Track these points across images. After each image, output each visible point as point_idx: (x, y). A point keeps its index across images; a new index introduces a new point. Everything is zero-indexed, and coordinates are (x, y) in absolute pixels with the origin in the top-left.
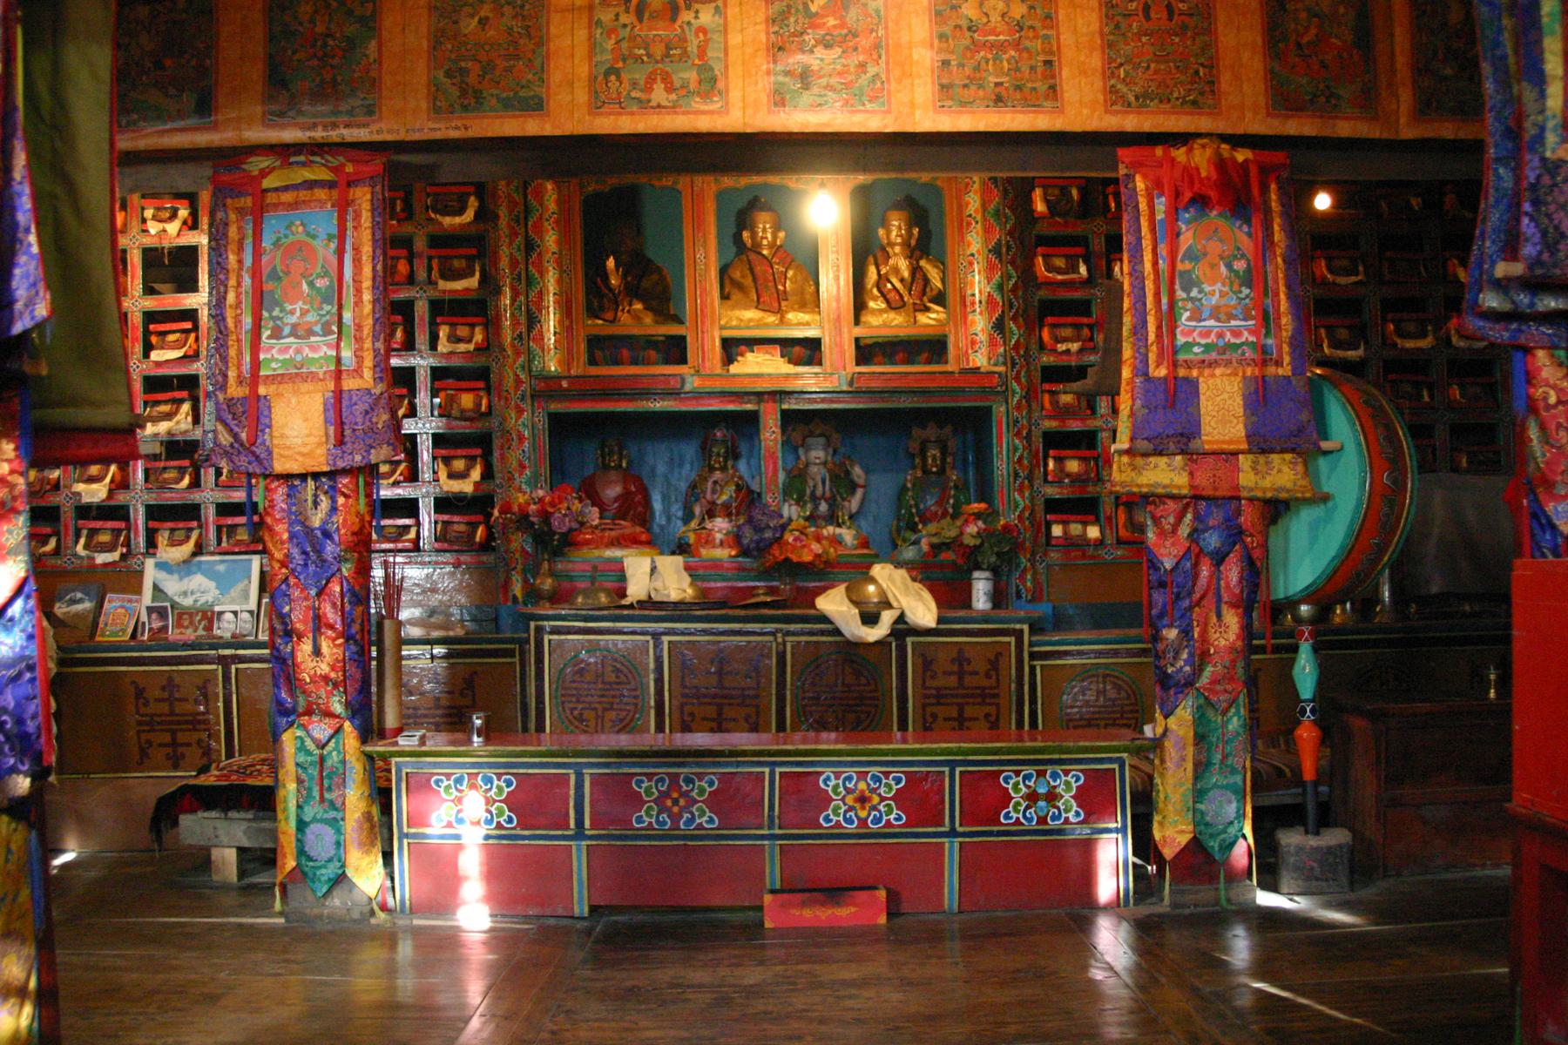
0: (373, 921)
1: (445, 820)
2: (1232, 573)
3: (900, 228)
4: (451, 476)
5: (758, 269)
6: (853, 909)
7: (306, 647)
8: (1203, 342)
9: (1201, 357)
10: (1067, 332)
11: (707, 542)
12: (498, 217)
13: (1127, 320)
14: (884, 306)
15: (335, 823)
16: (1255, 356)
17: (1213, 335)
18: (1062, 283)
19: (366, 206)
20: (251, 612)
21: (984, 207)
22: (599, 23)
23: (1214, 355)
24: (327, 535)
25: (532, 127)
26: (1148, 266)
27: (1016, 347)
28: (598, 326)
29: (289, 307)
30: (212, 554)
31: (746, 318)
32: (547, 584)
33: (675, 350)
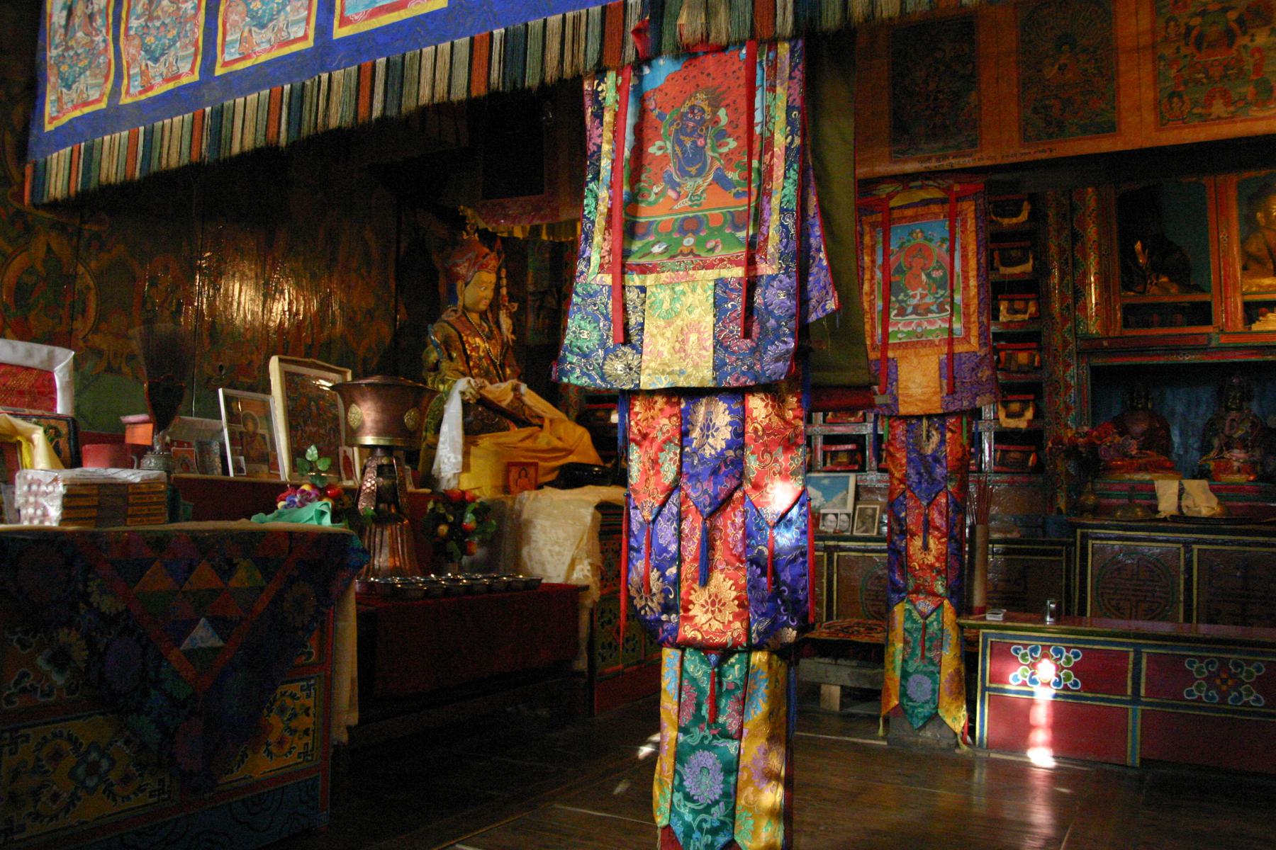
0: (957, 751)
1: (1021, 679)
4: (1009, 416)
7: (918, 542)
12: (1047, 215)
15: (932, 675)
20: (848, 515)
22: (1161, 57)
24: (936, 460)
25: (1106, 145)
29: (911, 293)
30: (819, 471)
32: (1091, 500)
33: (1202, 314)
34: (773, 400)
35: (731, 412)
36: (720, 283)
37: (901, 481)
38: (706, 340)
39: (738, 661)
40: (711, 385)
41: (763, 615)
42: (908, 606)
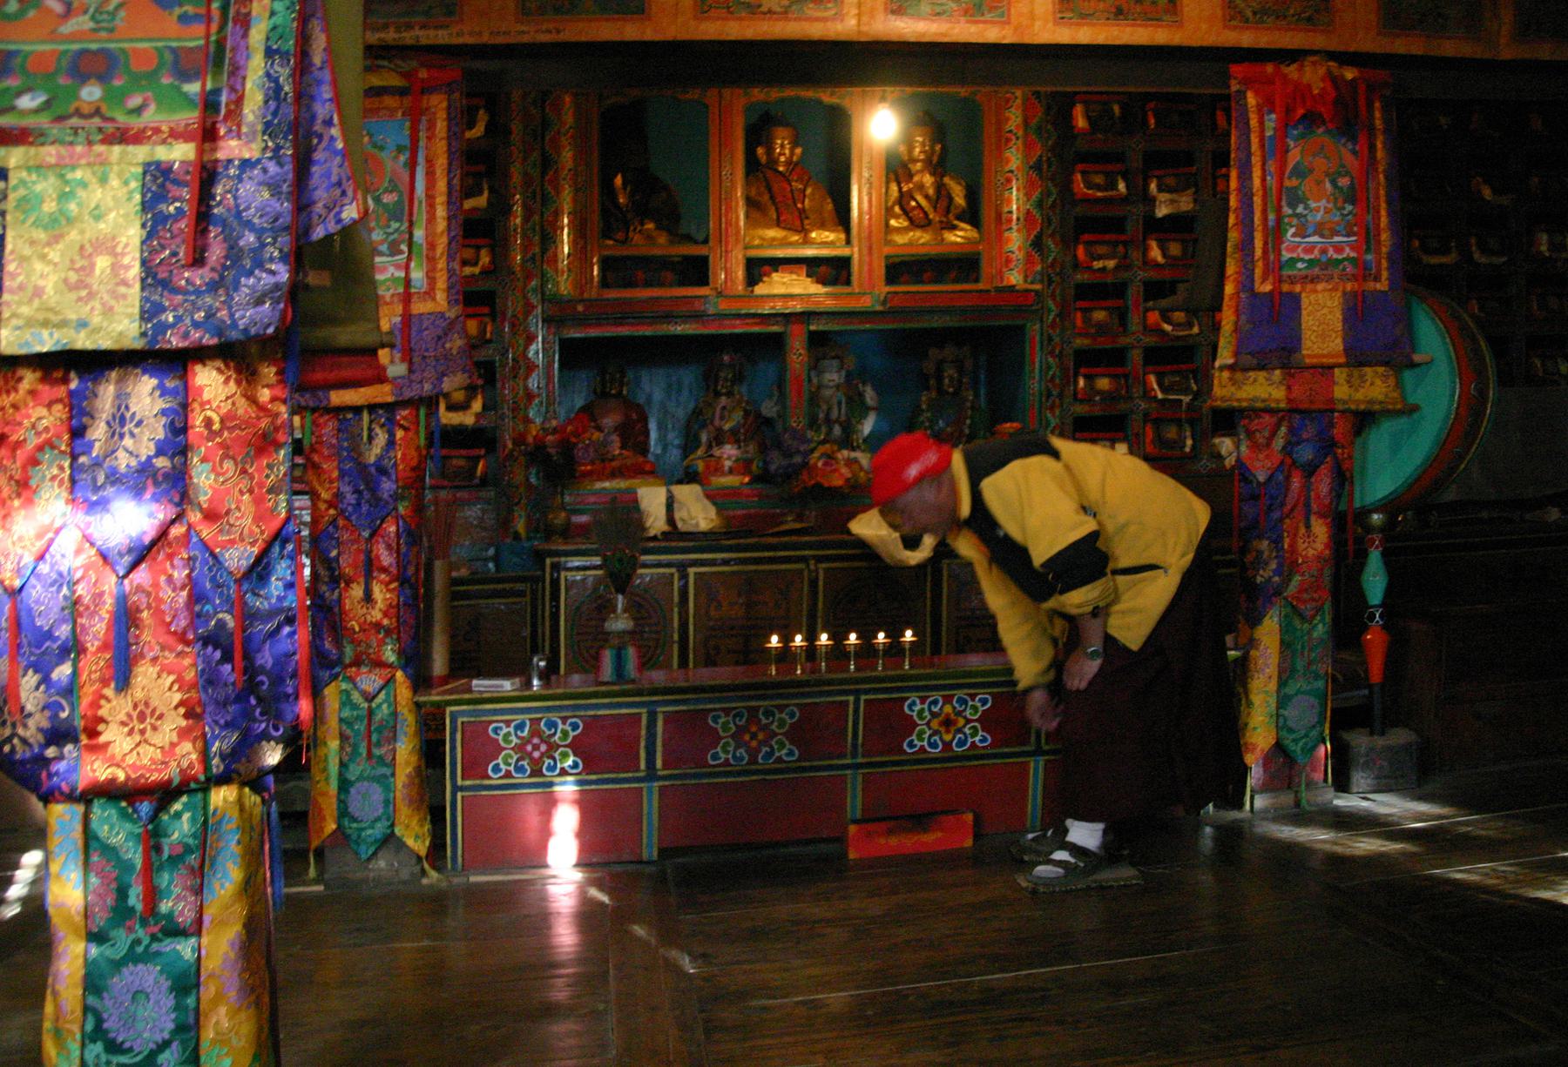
0: (425, 881)
2: (1323, 484)
3: (923, 144)
5: (776, 188)
6: (940, 834)
7: (357, 591)
8: (1307, 257)
9: (1304, 272)
10: (1101, 250)
11: (716, 470)
13: (1233, 236)
14: (906, 224)
15: (383, 781)
16: (1355, 271)
17: (1316, 252)
18: (1098, 200)
19: (442, 115)
21: (1026, 122)
23: (1317, 270)
24: (383, 471)
25: (631, 31)
26: (1257, 182)
27: (1052, 265)
28: (611, 248)
31: (772, 239)
33: (697, 271)
34: (239, 371)
35: (164, 392)
36: (159, 173)
37: (331, 504)
38: (128, 268)
39: (186, 807)
40: (139, 345)
41: (227, 725)
42: (344, 686)
